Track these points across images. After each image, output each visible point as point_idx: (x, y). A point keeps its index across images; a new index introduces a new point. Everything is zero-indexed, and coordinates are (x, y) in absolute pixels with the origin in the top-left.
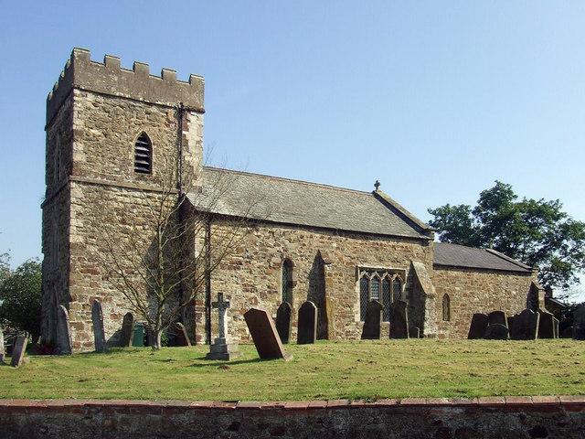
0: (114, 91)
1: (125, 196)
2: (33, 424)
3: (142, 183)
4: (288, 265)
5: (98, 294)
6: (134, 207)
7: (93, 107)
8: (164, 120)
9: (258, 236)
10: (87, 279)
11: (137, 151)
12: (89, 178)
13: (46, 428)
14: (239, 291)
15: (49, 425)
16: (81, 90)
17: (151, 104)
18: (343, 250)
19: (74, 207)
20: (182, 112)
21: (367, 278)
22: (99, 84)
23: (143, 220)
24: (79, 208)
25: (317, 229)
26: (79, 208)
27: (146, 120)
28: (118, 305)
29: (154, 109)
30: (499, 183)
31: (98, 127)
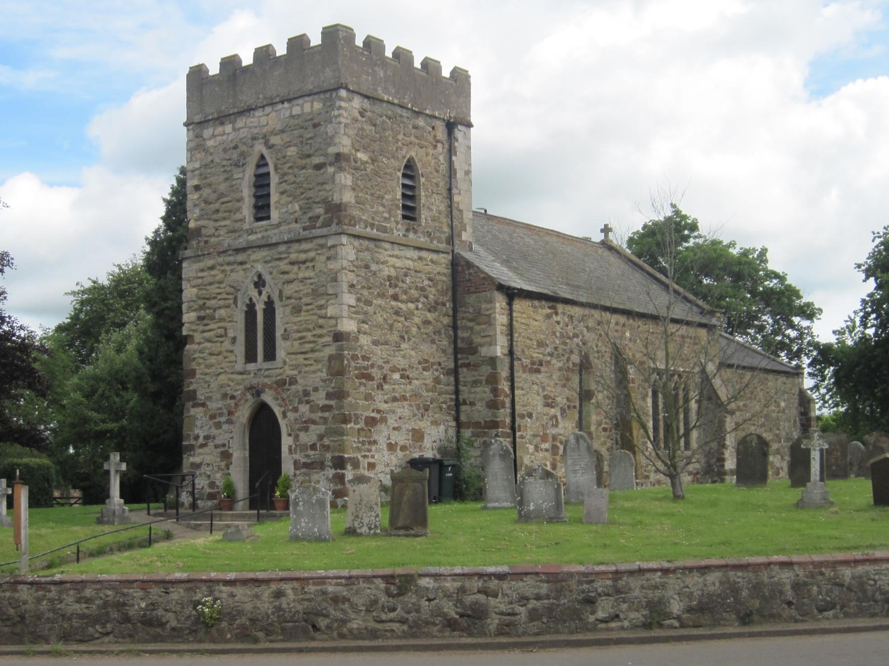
0: (380, 93)
1: (397, 257)
2: (860, 577)
3: (411, 235)
4: (584, 366)
5: (373, 411)
6: (406, 275)
7: (360, 118)
8: (431, 139)
9: (558, 323)
10: (362, 389)
11: (404, 186)
12: (358, 229)
13: (874, 580)
14: (540, 408)
15: (877, 577)
16: (348, 90)
17: (418, 114)
18: (635, 341)
19: (346, 274)
20: (450, 127)
21: (264, 361)
22: (365, 83)
23: (414, 293)
24: (351, 277)
25: (614, 311)
26: (351, 277)
27: (413, 138)
28: (394, 429)
29: (421, 122)
30: (677, 213)
31: (365, 148)
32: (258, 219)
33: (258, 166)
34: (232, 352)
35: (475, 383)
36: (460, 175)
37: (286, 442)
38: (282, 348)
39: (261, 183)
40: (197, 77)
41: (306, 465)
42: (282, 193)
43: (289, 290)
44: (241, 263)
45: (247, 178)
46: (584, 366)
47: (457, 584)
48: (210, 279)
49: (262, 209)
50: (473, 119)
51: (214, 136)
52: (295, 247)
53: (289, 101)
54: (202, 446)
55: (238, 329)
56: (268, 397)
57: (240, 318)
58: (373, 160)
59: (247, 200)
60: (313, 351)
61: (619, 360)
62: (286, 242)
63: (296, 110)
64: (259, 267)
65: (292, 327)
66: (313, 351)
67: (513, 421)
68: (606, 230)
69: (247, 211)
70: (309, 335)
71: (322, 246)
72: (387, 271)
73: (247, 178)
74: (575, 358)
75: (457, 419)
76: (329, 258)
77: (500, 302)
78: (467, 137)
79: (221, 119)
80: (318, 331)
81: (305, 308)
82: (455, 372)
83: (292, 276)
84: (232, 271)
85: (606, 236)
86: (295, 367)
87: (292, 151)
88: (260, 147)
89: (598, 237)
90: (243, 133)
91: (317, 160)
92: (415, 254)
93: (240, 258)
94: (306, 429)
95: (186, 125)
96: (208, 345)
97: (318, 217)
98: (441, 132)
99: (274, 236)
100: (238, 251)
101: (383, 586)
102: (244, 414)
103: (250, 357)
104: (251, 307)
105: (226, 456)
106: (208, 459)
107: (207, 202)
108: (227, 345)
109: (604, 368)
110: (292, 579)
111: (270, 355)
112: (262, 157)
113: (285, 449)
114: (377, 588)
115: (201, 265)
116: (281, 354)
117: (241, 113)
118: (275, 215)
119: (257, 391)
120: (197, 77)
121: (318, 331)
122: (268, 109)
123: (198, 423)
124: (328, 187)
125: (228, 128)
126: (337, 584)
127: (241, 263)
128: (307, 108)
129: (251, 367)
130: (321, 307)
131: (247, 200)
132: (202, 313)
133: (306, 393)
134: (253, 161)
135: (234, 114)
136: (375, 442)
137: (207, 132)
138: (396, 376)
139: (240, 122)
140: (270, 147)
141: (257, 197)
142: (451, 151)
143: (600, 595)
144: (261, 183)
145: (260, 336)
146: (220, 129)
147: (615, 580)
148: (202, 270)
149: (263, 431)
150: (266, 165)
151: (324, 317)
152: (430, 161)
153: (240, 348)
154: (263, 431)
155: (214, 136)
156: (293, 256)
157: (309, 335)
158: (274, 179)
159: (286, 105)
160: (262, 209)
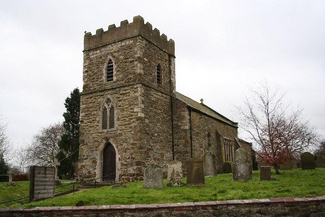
32: (108, 81)
33: (109, 63)
34: (98, 125)
35: (180, 138)
36: (172, 72)
37: (118, 156)
38: (116, 123)
39: (110, 69)
40: (88, 36)
41: (125, 165)
42: (117, 71)
43: (120, 103)
44: (102, 95)
45: (105, 67)
46: (209, 135)
47: (247, 209)
48: (90, 101)
49: (110, 76)
50: (176, 55)
51: (93, 54)
52: (122, 89)
53: (121, 41)
54: (85, 159)
55: (99, 118)
56: (111, 141)
57: (100, 113)
58: (149, 62)
59: (104, 74)
60: (128, 124)
61: (218, 135)
62: (119, 87)
63: (123, 44)
64: (109, 96)
65: (120, 116)
66: (128, 124)
67: (192, 152)
68: (202, 100)
69: (104, 78)
70: (127, 119)
71: (133, 88)
72: (153, 99)
73: (105, 67)
74: (207, 133)
75: (173, 151)
76: (135, 92)
77: (186, 113)
78: (174, 61)
79: (96, 49)
80: (131, 117)
81: (126, 110)
82: (172, 135)
83: (121, 99)
84: (99, 98)
85: (202, 102)
86: (121, 130)
87: (122, 57)
88: (110, 57)
89: (200, 102)
90: (103, 53)
91: (130, 60)
92: (160, 94)
93: (102, 94)
94: (125, 152)
95: (83, 52)
96: (89, 124)
97: (131, 78)
98: (167, 57)
99: (115, 85)
100: (100, 91)
101: (211, 211)
102: (102, 147)
103: (104, 127)
104: (105, 109)
105: (95, 162)
106: (88, 163)
107: (90, 76)
108: (96, 123)
109: (213, 135)
110: (164, 208)
111: (112, 126)
112: (110, 60)
113: (117, 159)
114: (209, 212)
115: (88, 97)
116: (116, 126)
117: (103, 46)
118: (115, 78)
119: (107, 139)
120: (88, 36)
121: (131, 117)
122: (113, 44)
123: (84, 150)
124: (135, 68)
125: (98, 52)
126: (188, 210)
127: (102, 95)
128: (128, 43)
129: (105, 131)
130: (131, 109)
131: (104, 74)
132: (87, 113)
133: (126, 139)
134: (107, 61)
135: (101, 47)
136: (150, 157)
137: (91, 54)
138: (156, 135)
139: (103, 49)
140: (114, 57)
141: (108, 70)
142: (170, 64)
143: (311, 213)
144: (110, 69)
145: (108, 122)
146: (95, 52)
147: (317, 205)
148: (88, 99)
149: (108, 153)
150: (112, 63)
151: (134, 112)
152: (164, 65)
153: (100, 125)
154: (108, 153)
155: (93, 54)
156: (121, 92)
157: (127, 119)
158: (115, 67)
159: (120, 43)
160: (110, 76)
